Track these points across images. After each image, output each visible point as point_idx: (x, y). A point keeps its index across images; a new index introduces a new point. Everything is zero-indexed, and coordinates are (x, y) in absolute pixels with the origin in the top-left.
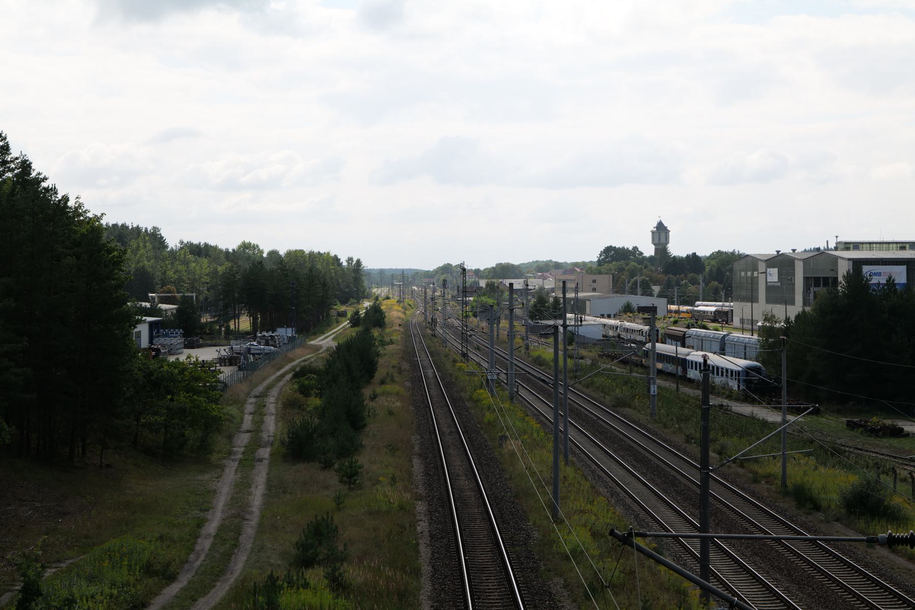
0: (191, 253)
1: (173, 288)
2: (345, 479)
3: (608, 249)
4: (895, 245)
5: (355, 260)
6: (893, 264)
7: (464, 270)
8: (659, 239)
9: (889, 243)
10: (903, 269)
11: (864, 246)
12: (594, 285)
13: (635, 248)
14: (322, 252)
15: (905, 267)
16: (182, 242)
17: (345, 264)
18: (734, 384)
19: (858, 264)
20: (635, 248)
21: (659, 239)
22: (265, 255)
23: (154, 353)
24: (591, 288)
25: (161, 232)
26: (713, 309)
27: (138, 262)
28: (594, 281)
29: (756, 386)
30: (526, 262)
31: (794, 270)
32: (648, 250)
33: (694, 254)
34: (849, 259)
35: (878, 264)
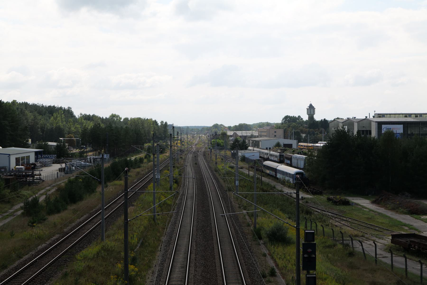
0: (84, 119)
1: (72, 135)
2: (30, 224)
3: (286, 117)
4: (401, 115)
5: (164, 122)
6: (392, 124)
7: (173, 127)
8: (310, 112)
9: (390, 114)
10: (401, 126)
11: (388, 115)
12: (275, 134)
13: (299, 117)
14: (149, 118)
15: (402, 125)
16: (81, 114)
17: (160, 124)
18: (291, 180)
19: (380, 124)
20: (299, 117)
21: (310, 112)
22: (122, 120)
23: (33, 166)
24: (274, 135)
25: (72, 109)
26: (322, 145)
27: (57, 123)
28: (275, 132)
29: (301, 182)
30: (256, 123)
31: (354, 127)
32: (305, 118)
33: (325, 119)
34: (376, 122)
35: (390, 124)
